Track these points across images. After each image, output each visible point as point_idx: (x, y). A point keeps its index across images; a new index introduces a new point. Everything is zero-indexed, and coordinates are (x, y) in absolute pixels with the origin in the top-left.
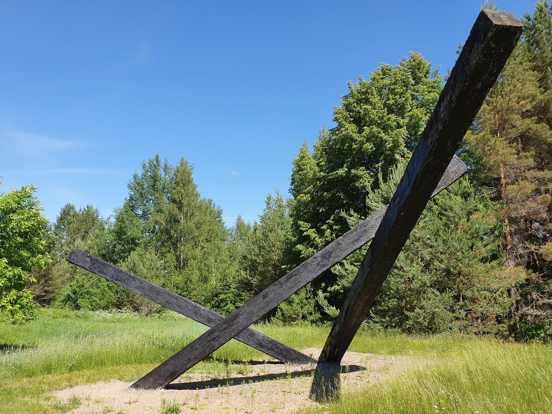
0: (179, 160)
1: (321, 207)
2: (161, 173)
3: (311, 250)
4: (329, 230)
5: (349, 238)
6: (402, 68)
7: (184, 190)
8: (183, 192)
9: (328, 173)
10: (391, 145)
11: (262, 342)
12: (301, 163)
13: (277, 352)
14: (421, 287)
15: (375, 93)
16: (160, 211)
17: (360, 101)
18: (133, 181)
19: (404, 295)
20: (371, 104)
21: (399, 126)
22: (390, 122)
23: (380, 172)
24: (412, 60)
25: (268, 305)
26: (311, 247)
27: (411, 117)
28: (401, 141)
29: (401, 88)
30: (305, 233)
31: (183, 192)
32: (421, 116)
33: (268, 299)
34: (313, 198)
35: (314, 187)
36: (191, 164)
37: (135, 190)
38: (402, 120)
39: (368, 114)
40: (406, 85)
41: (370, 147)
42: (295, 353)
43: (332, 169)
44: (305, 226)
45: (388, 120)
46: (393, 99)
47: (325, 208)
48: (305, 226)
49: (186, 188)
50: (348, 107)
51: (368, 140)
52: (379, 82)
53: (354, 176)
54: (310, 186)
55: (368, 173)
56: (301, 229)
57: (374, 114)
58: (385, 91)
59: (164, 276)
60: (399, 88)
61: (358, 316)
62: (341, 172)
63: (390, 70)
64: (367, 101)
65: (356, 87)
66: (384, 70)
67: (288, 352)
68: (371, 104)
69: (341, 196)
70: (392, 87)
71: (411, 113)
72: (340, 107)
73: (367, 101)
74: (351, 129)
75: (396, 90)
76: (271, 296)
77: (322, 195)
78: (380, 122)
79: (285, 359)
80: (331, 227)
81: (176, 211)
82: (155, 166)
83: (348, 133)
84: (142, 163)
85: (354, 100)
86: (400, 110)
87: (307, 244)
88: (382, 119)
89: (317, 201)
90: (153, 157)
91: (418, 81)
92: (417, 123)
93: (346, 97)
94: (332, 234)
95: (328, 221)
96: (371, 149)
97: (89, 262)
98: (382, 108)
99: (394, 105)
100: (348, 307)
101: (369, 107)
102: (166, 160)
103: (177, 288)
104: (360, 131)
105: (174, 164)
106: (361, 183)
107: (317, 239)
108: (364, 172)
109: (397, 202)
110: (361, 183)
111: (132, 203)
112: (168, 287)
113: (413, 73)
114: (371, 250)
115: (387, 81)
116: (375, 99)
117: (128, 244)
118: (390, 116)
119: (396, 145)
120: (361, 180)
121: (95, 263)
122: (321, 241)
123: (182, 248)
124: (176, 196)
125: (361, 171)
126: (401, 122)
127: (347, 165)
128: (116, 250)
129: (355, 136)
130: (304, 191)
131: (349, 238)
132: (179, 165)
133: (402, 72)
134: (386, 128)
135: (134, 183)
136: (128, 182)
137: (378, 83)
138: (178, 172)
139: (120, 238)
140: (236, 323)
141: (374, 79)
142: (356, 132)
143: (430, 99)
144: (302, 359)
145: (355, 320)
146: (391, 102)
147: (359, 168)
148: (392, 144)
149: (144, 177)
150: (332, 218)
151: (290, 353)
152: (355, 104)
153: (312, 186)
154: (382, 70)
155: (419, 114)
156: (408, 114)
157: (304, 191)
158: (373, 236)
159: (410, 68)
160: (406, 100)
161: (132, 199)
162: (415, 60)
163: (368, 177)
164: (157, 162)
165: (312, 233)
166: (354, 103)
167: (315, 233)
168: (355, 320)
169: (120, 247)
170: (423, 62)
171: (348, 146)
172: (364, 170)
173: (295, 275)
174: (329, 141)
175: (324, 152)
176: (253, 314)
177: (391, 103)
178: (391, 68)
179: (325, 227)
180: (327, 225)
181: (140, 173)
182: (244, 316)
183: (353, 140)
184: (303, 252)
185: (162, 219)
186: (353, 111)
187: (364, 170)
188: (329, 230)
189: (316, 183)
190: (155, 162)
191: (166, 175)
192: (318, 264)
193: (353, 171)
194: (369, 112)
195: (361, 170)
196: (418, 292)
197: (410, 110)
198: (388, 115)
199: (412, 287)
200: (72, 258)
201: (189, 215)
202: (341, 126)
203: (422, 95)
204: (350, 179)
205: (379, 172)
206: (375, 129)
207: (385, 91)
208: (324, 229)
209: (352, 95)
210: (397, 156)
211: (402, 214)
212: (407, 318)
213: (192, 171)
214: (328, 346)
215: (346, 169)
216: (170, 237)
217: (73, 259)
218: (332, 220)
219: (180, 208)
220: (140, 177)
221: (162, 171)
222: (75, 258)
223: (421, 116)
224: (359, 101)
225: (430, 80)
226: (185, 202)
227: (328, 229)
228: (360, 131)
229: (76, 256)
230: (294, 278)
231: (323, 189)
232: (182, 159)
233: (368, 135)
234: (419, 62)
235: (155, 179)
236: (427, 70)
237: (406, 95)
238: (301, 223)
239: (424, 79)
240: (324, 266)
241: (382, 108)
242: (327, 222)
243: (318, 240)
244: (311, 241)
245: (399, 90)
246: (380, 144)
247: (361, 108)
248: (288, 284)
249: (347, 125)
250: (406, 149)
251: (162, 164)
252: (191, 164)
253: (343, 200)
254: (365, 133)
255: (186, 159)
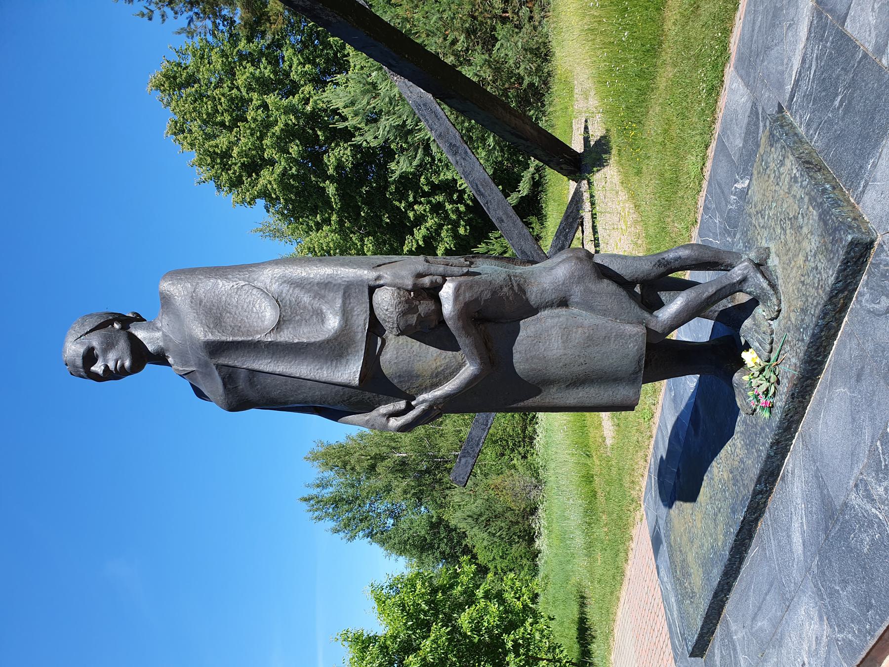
0: (309, 464)
1: (382, 220)
2: (327, 493)
3: (444, 234)
4: (415, 206)
5: (433, 124)
6: (174, 104)
7: (355, 452)
8: (357, 454)
9: (332, 209)
10: (292, 117)
11: (558, 247)
12: (319, 252)
13: (569, 229)
14: (490, 67)
15: (213, 143)
16: (388, 489)
17: (225, 165)
18: (342, 534)
19: (501, 90)
20: (230, 149)
21: (265, 106)
22: (259, 118)
23: (335, 126)
24: (162, 88)
25: (511, 217)
26: (439, 235)
27: (250, 89)
28: (285, 102)
29: (206, 103)
30: (421, 243)
31: (357, 454)
32: (247, 74)
33: (504, 218)
34: (368, 234)
35: (352, 232)
36: (314, 445)
37: (357, 530)
38: (254, 102)
39: (245, 151)
40: (200, 97)
41: (296, 148)
42: (570, 207)
43: (327, 203)
44: (411, 244)
45: (255, 120)
46: (222, 115)
47: (384, 215)
48: (411, 244)
49: (352, 451)
50: (236, 183)
51: (285, 150)
52: (196, 137)
53: (336, 171)
54: (351, 238)
55: (333, 150)
56: (415, 249)
57: (246, 142)
58: (209, 130)
59: (486, 475)
60: (205, 106)
61: (523, 123)
62: (331, 189)
63: (176, 123)
64: (226, 154)
65: (204, 173)
66: (176, 131)
67: (569, 216)
68: (230, 149)
69: (365, 191)
70: (205, 116)
71: (242, 90)
72: (233, 197)
73: (226, 154)
74: (267, 178)
75: (210, 111)
76: (500, 213)
77: (365, 219)
78: (258, 133)
79: (577, 219)
80: (410, 206)
81: (388, 463)
82: (318, 502)
83: (275, 180)
84: (315, 521)
85: (223, 174)
86: (239, 106)
87: (436, 240)
88: (252, 129)
89: (373, 227)
90: (305, 506)
91: (192, 80)
92: (258, 80)
93: (219, 187)
94: (420, 203)
95: (402, 208)
96: (297, 146)
97: (466, 459)
98: (238, 129)
99: (232, 114)
100: (512, 134)
101: (235, 151)
102: (308, 486)
103: (503, 455)
104: (272, 162)
105: (315, 472)
106: (347, 160)
107: (428, 225)
108: (332, 156)
109: (393, 63)
110: (347, 160)
111: (376, 534)
112: (502, 468)
113: (181, 86)
114: (446, 100)
115: (195, 126)
116: (223, 141)
117: (439, 533)
118: (249, 118)
119: (290, 110)
120: (343, 159)
121: (468, 452)
122: (431, 219)
123: (443, 452)
124: (365, 464)
125: (330, 160)
126: (256, 102)
127: (320, 183)
128: (448, 551)
129: (278, 169)
130: (359, 247)
131: (433, 124)
132: (315, 463)
133: (181, 103)
134: (267, 125)
135: (346, 532)
136: (345, 540)
137: (198, 139)
138: (327, 464)
139: (431, 546)
140: (531, 253)
141: (192, 145)
142: (273, 169)
143: (222, 61)
144: (577, 199)
145: (528, 128)
146: (227, 118)
147: (326, 164)
148: (291, 115)
149: (335, 518)
150: (397, 203)
151: (570, 213)
152: (230, 172)
153: (351, 236)
154: (175, 134)
155: (245, 77)
156: (244, 94)
157: (359, 247)
158: (430, 96)
159: (174, 90)
160: (223, 95)
161: (371, 535)
162: (161, 84)
163: (338, 150)
164: (312, 498)
165: (420, 234)
166: (229, 175)
167: (420, 229)
168: (528, 128)
169: (443, 545)
170: (164, 71)
171: (294, 180)
172: (328, 155)
173: (477, 185)
174: (282, 214)
175: (301, 220)
176: (520, 233)
177: (229, 118)
178: (173, 121)
179: (411, 214)
180: (408, 211)
181: (330, 524)
182: (522, 243)
183: (284, 173)
184: (447, 246)
185: (400, 485)
186: (241, 176)
187: (328, 155)
188: (416, 207)
189: (348, 228)
190: (311, 501)
191: (331, 485)
192: (464, 159)
193: (331, 171)
194: (242, 151)
195: (329, 161)
196: (497, 70)
197: (239, 89)
198: (248, 122)
199: (491, 78)
200: (461, 480)
201: (393, 444)
202: (265, 194)
203: (215, 72)
204: (342, 179)
205: (336, 127)
206: (267, 142)
207: (209, 130)
208: (414, 215)
209: (217, 177)
210: (309, 108)
211: (407, 56)
212: (531, 85)
213: (325, 443)
214: (562, 169)
215: (328, 182)
216: (428, 471)
217: (463, 478)
218: (401, 203)
219: (383, 459)
220: (335, 524)
221: (325, 491)
222: (462, 476)
223: (247, 74)
224: (226, 167)
225: (190, 61)
226: (374, 451)
227: (413, 210)
228: (272, 162)
229: (459, 476)
230: (479, 186)
231: (355, 219)
232: (307, 459)
233: (278, 152)
234: (165, 77)
235: (337, 502)
236: (175, 66)
237: (217, 97)
238: (406, 249)
239: (190, 70)
240: (466, 152)
241: (238, 129)
242: (403, 210)
243: (430, 223)
244: (432, 235)
245: (209, 107)
246: (289, 134)
247: (236, 164)
248: (486, 194)
249: (262, 182)
250: (297, 96)
251: (315, 491)
252: (314, 445)
253: (372, 187)
254: (276, 154)
255: (306, 453)
